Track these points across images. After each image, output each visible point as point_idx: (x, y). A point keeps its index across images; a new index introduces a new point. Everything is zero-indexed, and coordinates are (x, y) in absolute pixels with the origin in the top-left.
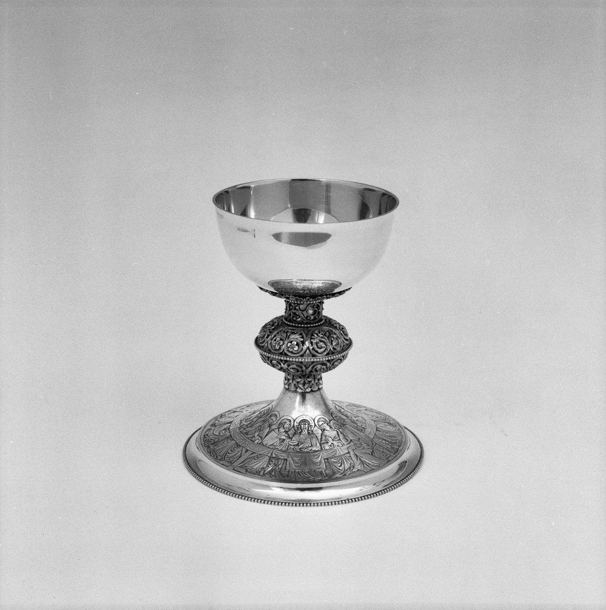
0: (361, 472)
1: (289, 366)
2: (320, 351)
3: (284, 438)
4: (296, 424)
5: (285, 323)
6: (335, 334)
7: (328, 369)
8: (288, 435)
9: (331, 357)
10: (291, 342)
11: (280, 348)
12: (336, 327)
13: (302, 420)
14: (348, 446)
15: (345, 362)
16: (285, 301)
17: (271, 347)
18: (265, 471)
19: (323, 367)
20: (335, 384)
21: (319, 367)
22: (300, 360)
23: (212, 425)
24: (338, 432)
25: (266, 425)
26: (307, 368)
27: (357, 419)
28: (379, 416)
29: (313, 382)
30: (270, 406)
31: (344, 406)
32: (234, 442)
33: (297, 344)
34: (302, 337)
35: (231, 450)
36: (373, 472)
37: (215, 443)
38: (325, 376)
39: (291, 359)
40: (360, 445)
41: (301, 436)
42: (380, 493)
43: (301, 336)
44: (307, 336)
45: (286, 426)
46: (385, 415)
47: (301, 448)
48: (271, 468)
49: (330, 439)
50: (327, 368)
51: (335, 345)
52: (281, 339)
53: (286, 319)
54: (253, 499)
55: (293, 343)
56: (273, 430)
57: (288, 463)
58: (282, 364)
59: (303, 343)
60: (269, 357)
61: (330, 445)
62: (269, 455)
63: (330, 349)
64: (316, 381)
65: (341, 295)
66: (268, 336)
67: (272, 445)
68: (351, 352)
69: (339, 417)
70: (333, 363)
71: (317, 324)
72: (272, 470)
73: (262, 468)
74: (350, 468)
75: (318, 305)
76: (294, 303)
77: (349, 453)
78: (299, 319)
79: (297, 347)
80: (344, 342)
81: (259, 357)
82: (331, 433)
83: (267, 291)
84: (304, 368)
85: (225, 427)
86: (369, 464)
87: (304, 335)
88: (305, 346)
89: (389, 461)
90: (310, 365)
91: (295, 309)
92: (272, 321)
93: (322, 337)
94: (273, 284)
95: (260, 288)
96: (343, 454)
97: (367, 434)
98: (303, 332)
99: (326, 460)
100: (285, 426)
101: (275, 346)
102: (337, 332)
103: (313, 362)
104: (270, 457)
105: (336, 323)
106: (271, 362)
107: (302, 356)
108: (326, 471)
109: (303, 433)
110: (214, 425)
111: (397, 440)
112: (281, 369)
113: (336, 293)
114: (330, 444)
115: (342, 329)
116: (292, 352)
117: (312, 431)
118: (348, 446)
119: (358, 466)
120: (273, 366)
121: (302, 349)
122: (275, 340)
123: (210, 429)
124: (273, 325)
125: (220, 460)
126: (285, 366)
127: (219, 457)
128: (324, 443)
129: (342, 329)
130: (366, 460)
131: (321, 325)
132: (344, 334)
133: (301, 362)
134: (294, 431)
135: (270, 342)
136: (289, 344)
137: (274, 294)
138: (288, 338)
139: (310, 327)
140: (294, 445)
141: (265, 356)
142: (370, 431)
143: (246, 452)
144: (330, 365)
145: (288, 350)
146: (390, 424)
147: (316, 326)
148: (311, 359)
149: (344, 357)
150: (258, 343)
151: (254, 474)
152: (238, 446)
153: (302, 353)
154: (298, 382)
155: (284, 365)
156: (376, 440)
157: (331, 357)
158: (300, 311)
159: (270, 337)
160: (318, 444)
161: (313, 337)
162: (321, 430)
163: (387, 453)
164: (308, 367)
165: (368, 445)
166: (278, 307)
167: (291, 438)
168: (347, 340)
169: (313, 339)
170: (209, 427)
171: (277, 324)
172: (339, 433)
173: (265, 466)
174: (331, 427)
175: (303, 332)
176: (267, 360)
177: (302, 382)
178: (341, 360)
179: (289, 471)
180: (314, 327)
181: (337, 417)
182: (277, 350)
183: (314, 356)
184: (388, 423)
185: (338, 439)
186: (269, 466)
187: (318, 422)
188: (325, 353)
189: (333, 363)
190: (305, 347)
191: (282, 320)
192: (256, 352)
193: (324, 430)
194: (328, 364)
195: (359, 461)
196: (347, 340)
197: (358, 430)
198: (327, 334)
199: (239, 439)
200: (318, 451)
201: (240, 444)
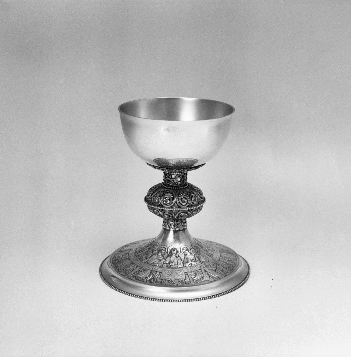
0: (208, 282)
1: (164, 213)
2: (183, 204)
3: (161, 259)
4: (169, 251)
5: (163, 187)
6: (194, 194)
7: (189, 216)
8: (164, 257)
9: (190, 208)
10: (165, 198)
11: (159, 202)
12: (195, 190)
13: (173, 248)
14: (201, 265)
15: (201, 213)
16: (164, 173)
17: (154, 201)
18: (147, 279)
19: (185, 214)
20: (193, 224)
21: (182, 214)
22: (171, 209)
23: (119, 251)
24: (195, 256)
25: (151, 251)
26: (175, 215)
27: (209, 249)
28: (224, 248)
29: (180, 225)
30: (154, 239)
31: (201, 241)
32: (130, 261)
33: (169, 200)
34: (173, 195)
35: (129, 268)
36: (215, 281)
37: (119, 262)
38: (188, 220)
39: (165, 209)
40: (208, 265)
41: (172, 258)
42: (219, 295)
43: (172, 194)
44: (175, 194)
45: (163, 251)
46: (228, 248)
47: (171, 266)
48: (151, 277)
49: (190, 260)
50: (188, 215)
51: (193, 201)
52: (159, 196)
53: (163, 184)
54: (134, 296)
55: (166, 199)
56: (155, 254)
57: (162, 275)
58: (160, 212)
59: (173, 199)
60: (152, 208)
61: (189, 264)
62: (151, 269)
63: (190, 203)
64: (182, 224)
65: (197, 169)
66: (152, 194)
67: (153, 263)
68: (205, 205)
69: (197, 247)
70: (192, 212)
71: (183, 188)
72: (152, 279)
73: (145, 277)
74: (201, 279)
75: (183, 176)
76: (168, 174)
77: (201, 269)
78: (171, 184)
79: (169, 201)
80: (199, 199)
81: (147, 208)
82: (191, 257)
83: (150, 165)
84: (173, 215)
85: (126, 252)
86: (213, 276)
87: (174, 193)
88: (174, 201)
89: (226, 275)
90: (177, 213)
91: (169, 177)
92: (156, 186)
93: (185, 196)
94: (157, 161)
95: (147, 164)
96: (197, 270)
97: (214, 258)
98: (175, 191)
99: (186, 273)
100: (162, 252)
101: (155, 201)
102: (195, 193)
103: (179, 211)
104: (151, 271)
105: (195, 187)
106: (153, 210)
107: (172, 207)
108: (186, 280)
109: (173, 256)
110: (120, 251)
111: (233, 263)
112: (159, 215)
113: (193, 167)
114: (189, 263)
115: (199, 191)
116: (166, 204)
117: (179, 255)
118: (201, 265)
119: (206, 278)
120: (155, 213)
121: (172, 202)
122: (156, 197)
123: (117, 254)
124: (155, 188)
125: (121, 272)
126: (162, 213)
127: (120, 270)
128: (185, 263)
129: (199, 192)
130: (211, 274)
131: (185, 188)
132: (200, 194)
133: (172, 211)
134: (167, 255)
135: (154, 199)
136: (164, 199)
137: (154, 167)
138: (164, 195)
139: (178, 189)
140: (167, 264)
141: (150, 207)
142: (217, 256)
143: (137, 267)
144: (191, 213)
145: (164, 203)
146: (230, 253)
147: (182, 189)
148: (177, 209)
149: (200, 209)
150: (146, 200)
151: (140, 281)
152: (133, 263)
153: (172, 205)
154: (171, 224)
155: (161, 212)
156: (219, 263)
157: (190, 208)
158: (171, 179)
159: (153, 195)
160: (182, 264)
161: (180, 195)
162: (184, 255)
163: (228, 270)
164: (176, 214)
165: (214, 265)
166: (158, 177)
167: (165, 259)
168: (202, 198)
169: (179, 196)
170: (117, 252)
171: (158, 187)
172: (196, 257)
173: (147, 276)
174: (191, 253)
175: (175, 191)
176: (152, 209)
177: (173, 224)
178: (197, 210)
179: (162, 280)
180: (180, 189)
181: (197, 247)
182: (157, 203)
183: (180, 207)
184: (229, 253)
185: (195, 260)
186: (150, 276)
187: (183, 249)
188: (187, 206)
189: (192, 212)
190: (174, 202)
191: (162, 185)
192: (145, 205)
193: (186, 255)
194: (189, 213)
195: (207, 275)
196: (202, 198)
197: (209, 256)
198: (189, 194)
199: (133, 258)
200: (181, 267)
201: (134, 262)
